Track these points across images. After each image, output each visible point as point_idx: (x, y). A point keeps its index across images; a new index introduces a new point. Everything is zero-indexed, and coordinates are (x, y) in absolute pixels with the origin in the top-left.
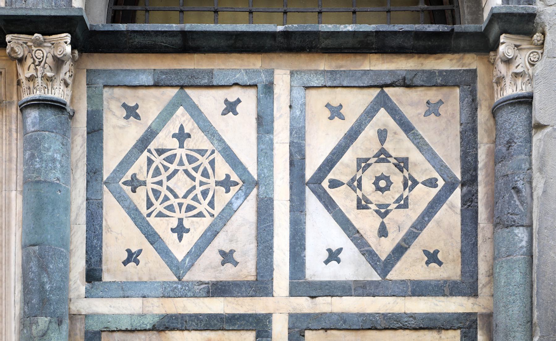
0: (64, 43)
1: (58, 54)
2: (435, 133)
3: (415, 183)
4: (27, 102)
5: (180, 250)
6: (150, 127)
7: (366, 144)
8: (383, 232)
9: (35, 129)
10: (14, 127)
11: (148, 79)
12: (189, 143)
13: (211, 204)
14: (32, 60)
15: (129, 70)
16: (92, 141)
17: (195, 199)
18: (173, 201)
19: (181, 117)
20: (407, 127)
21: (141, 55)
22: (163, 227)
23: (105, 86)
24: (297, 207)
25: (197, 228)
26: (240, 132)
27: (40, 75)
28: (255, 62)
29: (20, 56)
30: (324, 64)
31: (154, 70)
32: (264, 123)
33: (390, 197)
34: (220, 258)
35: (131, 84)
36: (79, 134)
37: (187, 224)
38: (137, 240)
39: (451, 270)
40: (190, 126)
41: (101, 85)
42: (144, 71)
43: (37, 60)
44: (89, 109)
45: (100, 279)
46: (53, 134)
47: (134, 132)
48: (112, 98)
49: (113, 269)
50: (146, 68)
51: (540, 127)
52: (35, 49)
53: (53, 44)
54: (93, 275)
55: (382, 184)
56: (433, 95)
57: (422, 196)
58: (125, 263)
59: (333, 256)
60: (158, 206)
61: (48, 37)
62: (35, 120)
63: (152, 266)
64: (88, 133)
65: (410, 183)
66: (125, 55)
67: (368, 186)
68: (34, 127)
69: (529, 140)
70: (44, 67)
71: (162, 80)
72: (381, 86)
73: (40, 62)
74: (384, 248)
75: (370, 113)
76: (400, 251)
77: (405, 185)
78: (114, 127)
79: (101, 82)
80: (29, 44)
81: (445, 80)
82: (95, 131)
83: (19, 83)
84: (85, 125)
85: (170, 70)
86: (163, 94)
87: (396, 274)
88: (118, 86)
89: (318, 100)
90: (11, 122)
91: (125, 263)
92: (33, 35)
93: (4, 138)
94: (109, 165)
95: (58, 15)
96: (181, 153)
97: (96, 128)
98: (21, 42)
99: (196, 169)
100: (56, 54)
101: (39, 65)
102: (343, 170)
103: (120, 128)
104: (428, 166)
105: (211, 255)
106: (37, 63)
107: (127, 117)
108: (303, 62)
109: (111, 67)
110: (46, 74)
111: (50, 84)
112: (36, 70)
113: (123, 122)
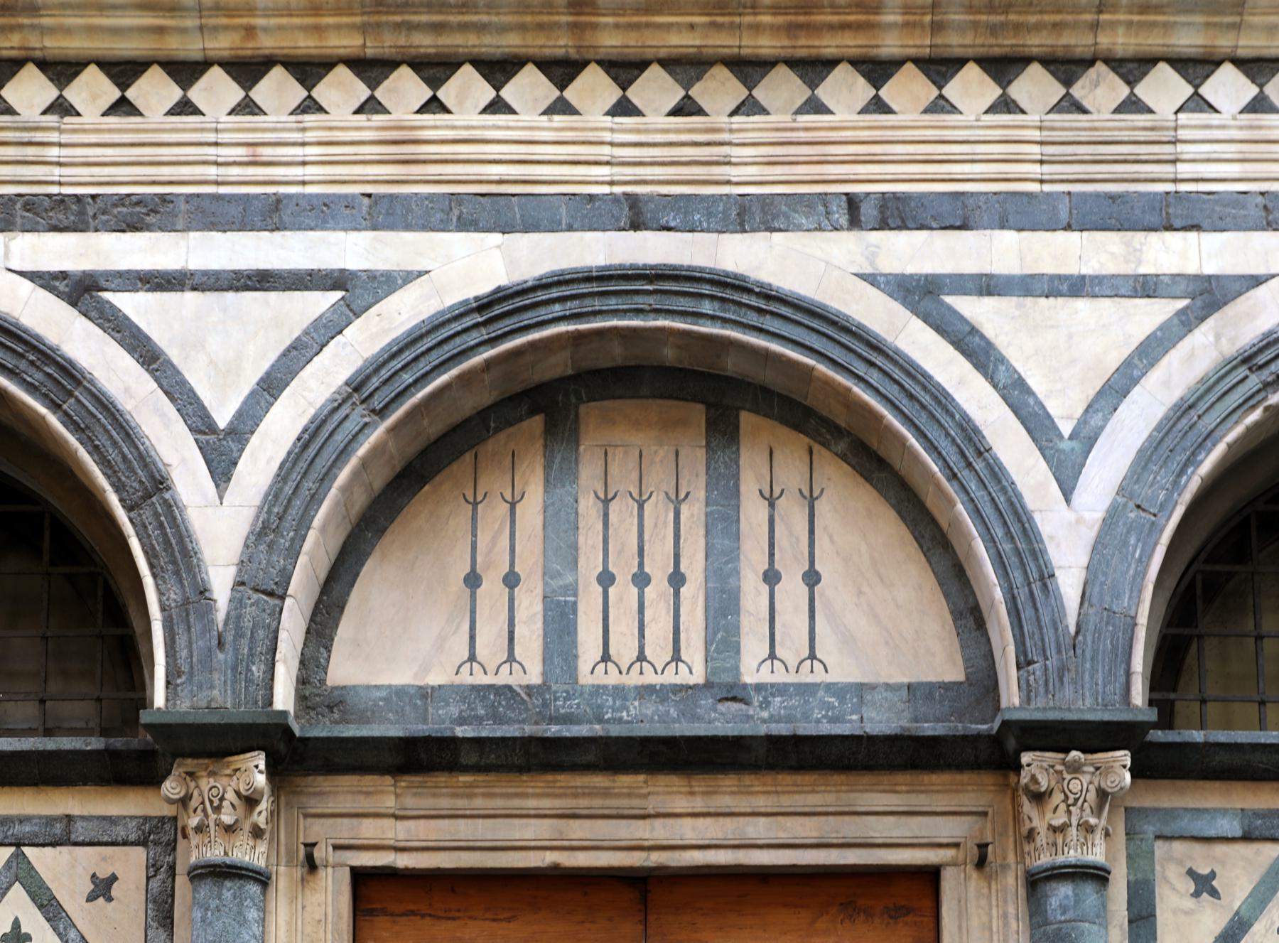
1: (1109, 784)
4: (1053, 868)
6: (1237, 913)
9: (1067, 917)
10: (1011, 909)
11: (1230, 826)
14: (1062, 797)
15: (1198, 810)
16: (1138, 936)
21: (1217, 784)
23: (1158, 837)
27: (1074, 823)
29: (1043, 789)
31: (1242, 810)
35: (1202, 834)
36: (1115, 922)
41: (1152, 836)
43: (1072, 797)
44: (1132, 878)
46: (1095, 928)
48: (1170, 858)
50: (1228, 806)
52: (1068, 777)
53: (1097, 769)
61: (1090, 756)
62: (1066, 902)
64: (1130, 922)
66: (1191, 783)
68: (1063, 913)
70: (1082, 809)
71: (1256, 828)
73: (1076, 800)
78: (1174, 912)
79: (1150, 829)
80: (1059, 767)
83: (1031, 836)
84: (1125, 907)
85: (1269, 810)
86: (1258, 853)
88: (1182, 838)
90: (1005, 901)
92: (1067, 751)
93: (995, 929)
95: (1115, 719)
97: (1144, 913)
98: (1045, 765)
100: (1103, 785)
101: (1074, 805)
103: (1187, 913)
106: (1071, 801)
107: (1196, 894)
109: (1167, 805)
110: (1087, 822)
111: (1090, 837)
112: (1069, 812)
113: (1189, 903)
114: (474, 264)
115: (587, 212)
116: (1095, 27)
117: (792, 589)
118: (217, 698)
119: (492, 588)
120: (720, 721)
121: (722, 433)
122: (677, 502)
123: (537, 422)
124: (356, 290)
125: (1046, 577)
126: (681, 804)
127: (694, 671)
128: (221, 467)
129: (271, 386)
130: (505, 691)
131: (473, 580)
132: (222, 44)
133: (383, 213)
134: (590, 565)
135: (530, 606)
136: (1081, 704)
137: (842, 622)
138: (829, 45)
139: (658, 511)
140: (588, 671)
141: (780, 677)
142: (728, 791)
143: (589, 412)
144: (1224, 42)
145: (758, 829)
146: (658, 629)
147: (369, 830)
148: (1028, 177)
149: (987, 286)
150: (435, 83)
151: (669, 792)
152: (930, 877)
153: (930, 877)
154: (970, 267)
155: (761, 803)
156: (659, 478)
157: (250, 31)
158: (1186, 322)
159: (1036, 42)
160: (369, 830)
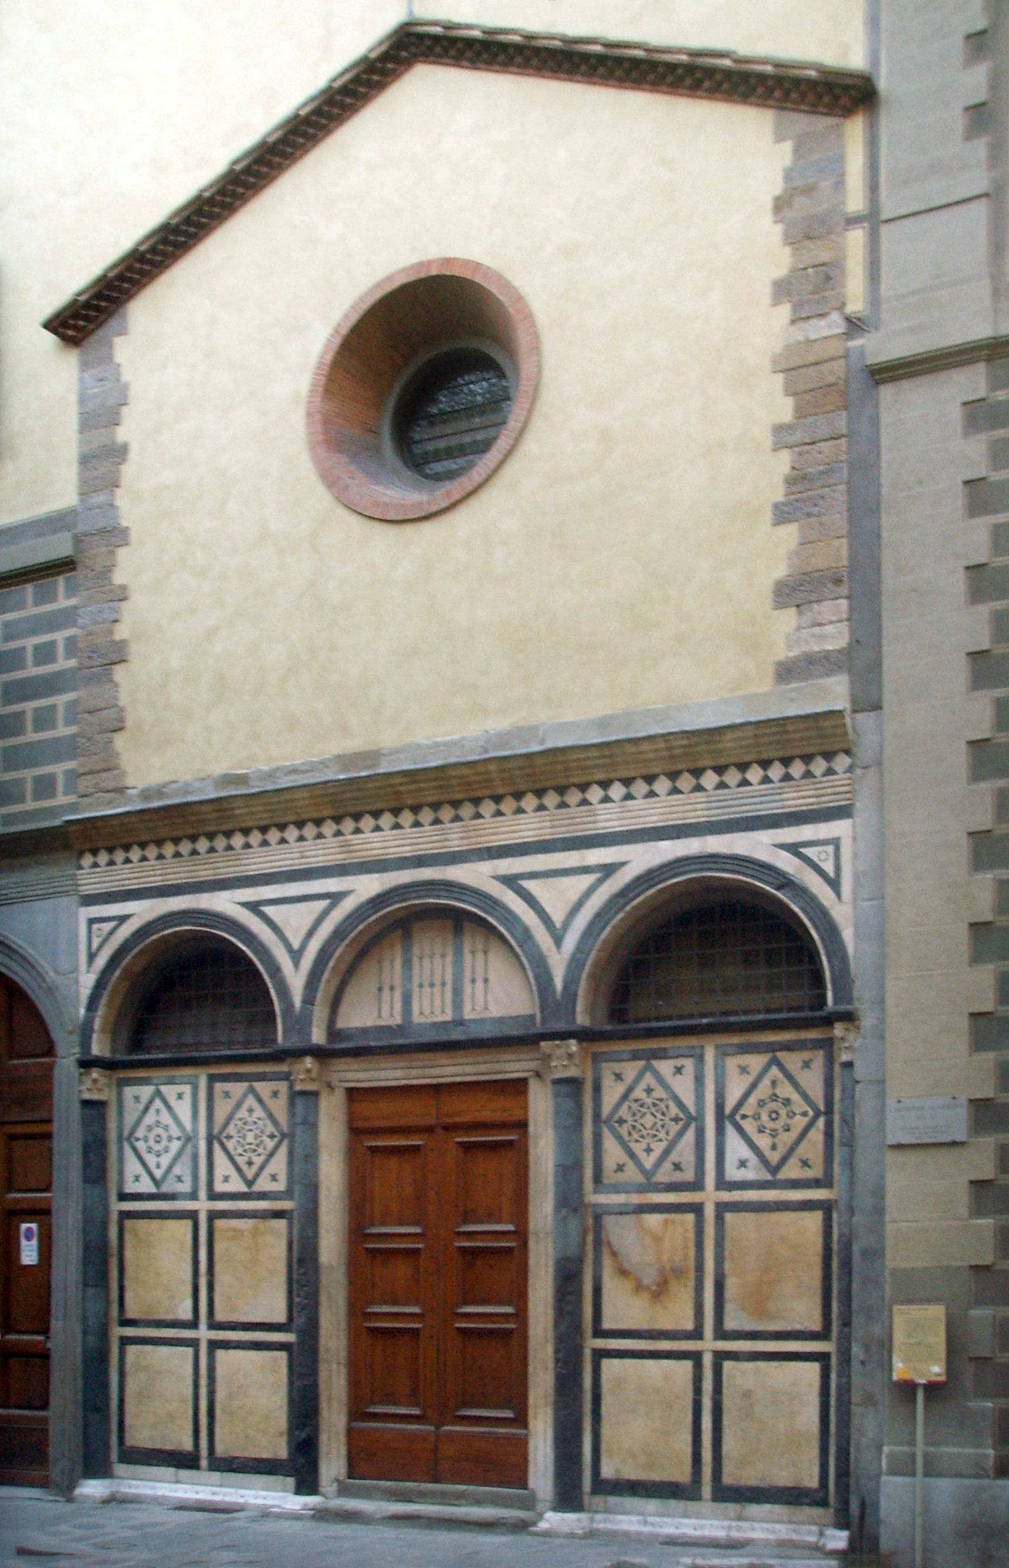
0: (308, 1062)
1: (569, 1051)
2: (492, 1266)
3: (795, 1114)
5: (648, 1162)
7: (764, 1089)
8: (774, 1147)
12: (655, 1095)
13: (667, 1133)
17: (657, 1130)
18: (644, 1132)
19: (649, 1079)
20: (169, 1108)
22: (638, 1148)
24: (720, 1131)
25: (659, 1148)
26: (684, 1087)
28: (693, 1041)
30: (735, 1039)
32: (699, 1080)
33: (778, 1125)
34: (672, 1167)
37: (652, 1146)
38: (622, 1157)
39: (816, 1172)
40: (654, 1084)
42: (624, 1051)
45: (601, 1182)
47: (620, 1089)
49: (609, 1175)
51: (858, 1082)
54: (597, 1179)
55: (774, 1116)
56: (806, 1055)
58: (616, 1171)
59: (743, 1164)
60: (635, 1136)
63: (632, 1174)
65: (791, 1115)
67: (765, 1117)
69: (853, 1090)
72: (774, 1051)
74: (774, 1157)
75: (766, 1069)
76: (784, 1160)
77: (788, 1116)
81: (816, 1045)
82: (597, 1089)
87: (782, 1175)
89: (732, 1063)
91: (616, 1171)
94: (606, 1110)
96: (649, 1101)
99: (657, 1111)
102: (748, 1109)
104: (803, 1103)
105: (667, 1165)
114: (367, 886)
115: (403, 863)
116: (567, 776)
117: (480, 984)
118: (294, 1042)
119: (386, 992)
120: (457, 1035)
121: (458, 931)
122: (443, 956)
123: (399, 933)
124: (335, 898)
125: (550, 979)
126: (446, 1062)
127: (448, 1016)
128: (296, 964)
129: (310, 934)
130: (389, 1027)
131: (380, 989)
132: (292, 818)
133: (342, 870)
134: (416, 980)
135: (398, 996)
136: (561, 1026)
137: (497, 994)
138: (479, 794)
139: (438, 961)
140: (417, 1018)
141: (478, 1017)
142: (460, 1057)
143: (416, 926)
144: (612, 776)
146: (437, 1003)
147: (350, 1075)
148: (546, 834)
149: (533, 875)
151: (442, 1058)
152: (523, 1082)
153: (523, 1082)
155: (471, 1060)
156: (438, 949)
157: (297, 813)
158: (600, 882)
159: (548, 784)
160: (350, 1075)
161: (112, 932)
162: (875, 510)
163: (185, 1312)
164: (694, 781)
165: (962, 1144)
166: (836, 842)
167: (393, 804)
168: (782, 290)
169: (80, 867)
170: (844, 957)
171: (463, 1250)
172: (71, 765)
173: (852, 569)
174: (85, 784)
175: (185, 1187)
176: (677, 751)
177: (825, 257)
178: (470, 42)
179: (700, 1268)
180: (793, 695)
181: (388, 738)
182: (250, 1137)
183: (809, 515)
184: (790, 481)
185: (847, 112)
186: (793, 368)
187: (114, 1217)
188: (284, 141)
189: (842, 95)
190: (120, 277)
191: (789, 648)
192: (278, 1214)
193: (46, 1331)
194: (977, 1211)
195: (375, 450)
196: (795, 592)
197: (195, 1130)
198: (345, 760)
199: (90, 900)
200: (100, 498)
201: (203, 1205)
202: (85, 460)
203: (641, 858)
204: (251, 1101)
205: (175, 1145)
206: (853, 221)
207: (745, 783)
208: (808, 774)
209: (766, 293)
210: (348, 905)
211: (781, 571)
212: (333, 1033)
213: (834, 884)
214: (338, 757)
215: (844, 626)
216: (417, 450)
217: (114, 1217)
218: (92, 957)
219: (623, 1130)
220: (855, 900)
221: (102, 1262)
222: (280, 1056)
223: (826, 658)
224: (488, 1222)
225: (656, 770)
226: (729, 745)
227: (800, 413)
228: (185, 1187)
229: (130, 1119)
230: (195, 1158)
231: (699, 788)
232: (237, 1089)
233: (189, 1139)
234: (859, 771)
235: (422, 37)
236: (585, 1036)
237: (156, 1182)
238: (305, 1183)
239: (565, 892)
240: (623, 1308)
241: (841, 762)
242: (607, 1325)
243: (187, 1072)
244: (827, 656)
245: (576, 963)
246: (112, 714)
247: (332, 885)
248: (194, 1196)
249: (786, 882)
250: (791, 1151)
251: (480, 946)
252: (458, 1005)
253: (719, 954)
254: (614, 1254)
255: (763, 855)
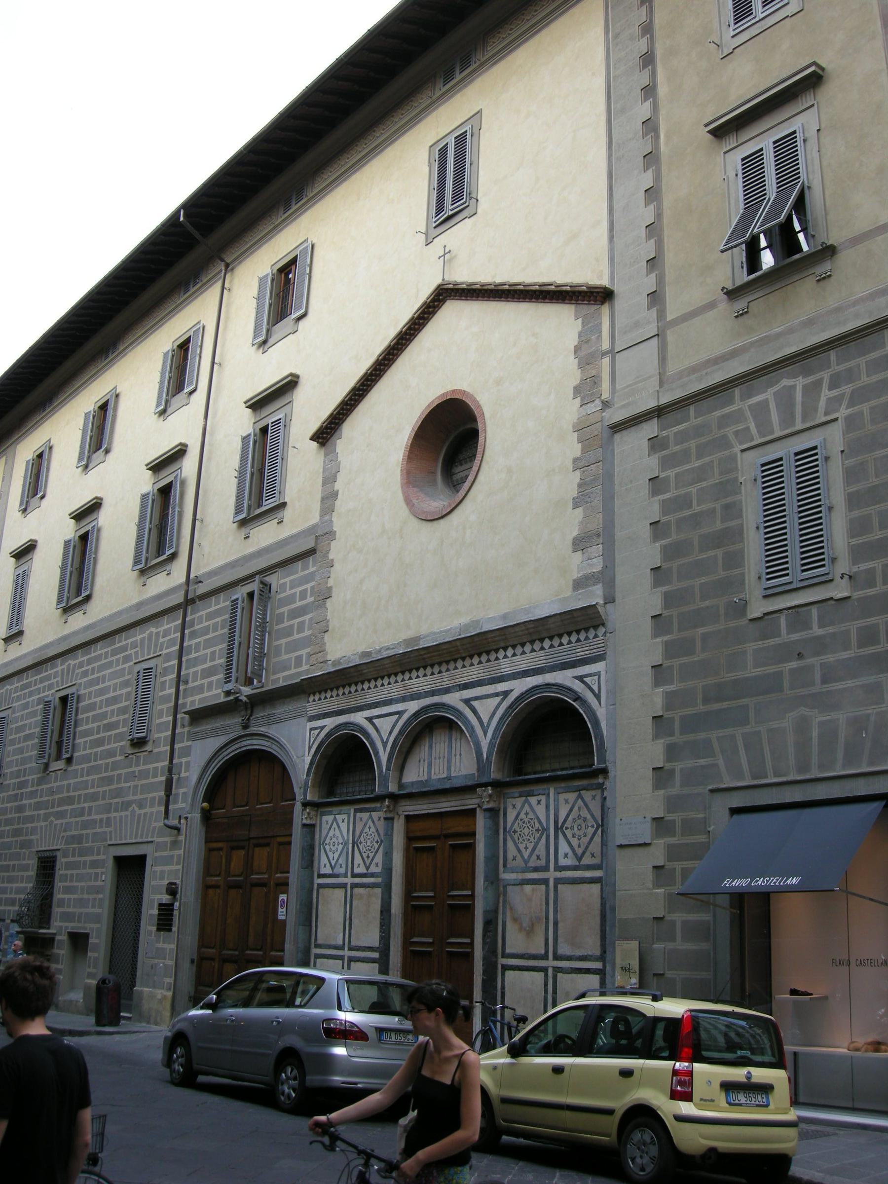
0: (490, 790)
8: (579, 846)
12: (529, 816)
20: (339, 827)
22: (522, 846)
25: (531, 846)
26: (541, 811)
28: (545, 786)
30: (563, 785)
32: (547, 807)
33: (581, 833)
38: (515, 853)
39: (596, 861)
40: (529, 810)
47: (515, 814)
54: (505, 866)
56: (593, 793)
57: (591, 830)
60: (521, 840)
65: (587, 827)
67: (575, 828)
74: (579, 851)
76: (584, 853)
89: (562, 797)
94: (509, 825)
105: (534, 857)
108: (558, 785)
114: (413, 707)
117: (458, 757)
119: (422, 762)
124: (400, 713)
127: (444, 776)
132: (385, 673)
133: (403, 699)
136: (484, 780)
138: (456, 657)
139: (442, 744)
140: (433, 777)
145: (453, 803)
148: (482, 676)
149: (476, 698)
150: (488, 655)
152: (475, 809)
154: (474, 695)
158: (503, 700)
161: (318, 735)
162: (613, 498)
163: (340, 942)
164: (550, 643)
165: (649, 844)
166: (598, 674)
167: (423, 664)
168: (577, 390)
169: (308, 702)
170: (602, 737)
171: (451, 906)
172: (308, 650)
173: (604, 528)
174: (313, 660)
175: (342, 871)
176: (532, 630)
177: (594, 373)
178: (463, 290)
179: (547, 918)
180: (580, 597)
181: (424, 630)
182: (369, 844)
183: (587, 502)
184: (580, 486)
185: (602, 303)
186: (580, 428)
187: (315, 886)
188: (397, 343)
189: (601, 296)
190: (339, 413)
191: (578, 573)
192: (592, 881)
193: (283, 950)
194: (657, 885)
195: (434, 483)
196: (580, 544)
197: (348, 839)
198: (407, 642)
199: (312, 718)
200: (327, 518)
201: (552, 875)
202: (323, 500)
203: (519, 686)
204: (370, 823)
205: (341, 847)
206: (604, 354)
207: (561, 644)
208: (587, 638)
209: (571, 392)
210: (405, 717)
211: (575, 533)
212: (401, 786)
213: (598, 696)
214: (405, 640)
215: (601, 559)
216: (455, 478)
217: (315, 886)
218: (310, 748)
219: (516, 837)
220: (607, 705)
221: (308, 913)
222: (380, 798)
223: (593, 576)
224: (462, 890)
225: (525, 640)
226: (552, 626)
227: (584, 451)
228: (342, 871)
229: (324, 833)
230: (347, 853)
231: (542, 648)
232: (365, 816)
233: (345, 844)
234: (608, 635)
235: (447, 289)
236: (497, 785)
237: (332, 868)
238: (388, 870)
239: (486, 706)
240: (515, 940)
241: (602, 630)
242: (508, 950)
243: (345, 808)
244: (593, 575)
245: (491, 744)
246: (323, 624)
247: (399, 707)
248: (346, 876)
249: (578, 698)
250: (587, 847)
251: (459, 737)
252: (449, 769)
253: (551, 739)
254: (511, 909)
255: (568, 683)
